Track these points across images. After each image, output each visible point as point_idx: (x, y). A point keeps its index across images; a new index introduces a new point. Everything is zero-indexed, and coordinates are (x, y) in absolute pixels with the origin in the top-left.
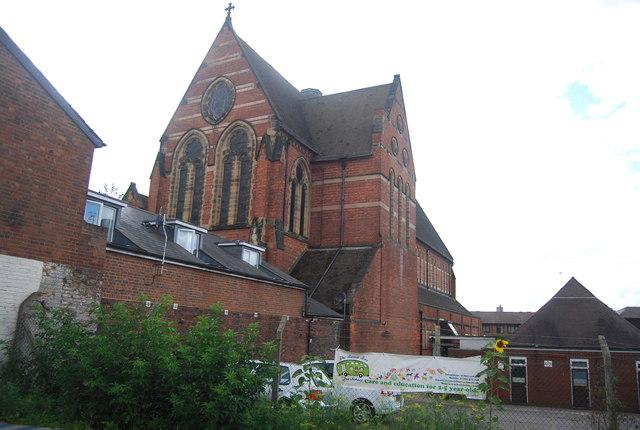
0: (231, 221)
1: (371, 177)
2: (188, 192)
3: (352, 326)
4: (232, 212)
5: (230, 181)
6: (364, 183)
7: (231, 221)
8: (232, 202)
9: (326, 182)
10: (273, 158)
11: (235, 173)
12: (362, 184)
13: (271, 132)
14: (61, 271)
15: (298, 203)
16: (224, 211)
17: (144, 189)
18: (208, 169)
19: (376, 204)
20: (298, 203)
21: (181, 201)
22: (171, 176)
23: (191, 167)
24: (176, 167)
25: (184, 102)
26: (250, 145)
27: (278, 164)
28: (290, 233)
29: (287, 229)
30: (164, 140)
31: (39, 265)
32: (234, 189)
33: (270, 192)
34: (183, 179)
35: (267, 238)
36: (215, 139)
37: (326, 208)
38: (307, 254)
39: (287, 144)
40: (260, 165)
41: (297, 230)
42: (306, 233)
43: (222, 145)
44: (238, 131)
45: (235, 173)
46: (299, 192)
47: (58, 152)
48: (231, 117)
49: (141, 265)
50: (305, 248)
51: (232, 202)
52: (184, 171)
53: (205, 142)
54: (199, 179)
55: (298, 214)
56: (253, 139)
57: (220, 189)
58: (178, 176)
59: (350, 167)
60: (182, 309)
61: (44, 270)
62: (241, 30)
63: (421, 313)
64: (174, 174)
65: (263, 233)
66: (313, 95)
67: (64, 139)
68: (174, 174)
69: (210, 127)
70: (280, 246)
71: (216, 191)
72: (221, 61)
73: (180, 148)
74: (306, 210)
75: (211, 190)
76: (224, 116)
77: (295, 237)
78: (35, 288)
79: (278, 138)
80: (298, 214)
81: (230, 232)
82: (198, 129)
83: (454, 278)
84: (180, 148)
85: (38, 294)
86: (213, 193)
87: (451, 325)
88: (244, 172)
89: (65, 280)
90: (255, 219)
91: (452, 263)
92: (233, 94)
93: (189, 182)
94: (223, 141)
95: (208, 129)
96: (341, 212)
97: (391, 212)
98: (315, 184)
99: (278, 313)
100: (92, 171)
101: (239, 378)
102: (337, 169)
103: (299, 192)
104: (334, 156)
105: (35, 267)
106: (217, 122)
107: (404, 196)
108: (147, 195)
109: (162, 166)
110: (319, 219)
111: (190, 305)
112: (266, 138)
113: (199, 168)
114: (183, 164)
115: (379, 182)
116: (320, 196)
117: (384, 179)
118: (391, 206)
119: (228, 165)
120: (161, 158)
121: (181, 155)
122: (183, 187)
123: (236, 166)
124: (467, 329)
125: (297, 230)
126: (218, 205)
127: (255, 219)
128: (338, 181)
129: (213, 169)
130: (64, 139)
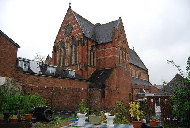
0: (73, 63)
1: (112, 48)
2: (62, 56)
3: (106, 91)
4: (73, 61)
5: (72, 52)
6: (110, 49)
7: (73, 63)
8: (73, 58)
9: (100, 50)
10: (83, 45)
11: (74, 50)
12: (110, 50)
13: (82, 37)
14: (10, 79)
15: (92, 57)
16: (71, 61)
17: (51, 56)
18: (67, 49)
19: (114, 55)
20: (92, 57)
21: (60, 59)
22: (57, 52)
23: (62, 49)
24: (58, 49)
25: (60, 31)
26: (77, 42)
27: (84, 47)
28: (93, 67)
29: (89, 64)
30: (55, 42)
31: (168, 83)
32: (73, 54)
33: (82, 54)
34: (61, 52)
35: (82, 67)
36: (68, 41)
37: (100, 58)
38: (95, 72)
39: (88, 40)
40: (79, 47)
41: (92, 64)
42: (95, 65)
43: (70, 42)
44: (74, 38)
45: (74, 50)
46: (92, 53)
47: (8, 50)
48: (72, 34)
49: (34, 76)
50: (95, 70)
51: (73, 58)
52: (61, 50)
53: (65, 42)
54: (64, 52)
55: (92, 60)
56: (77, 40)
57: (70, 55)
58: (59, 52)
59: (106, 45)
60: (48, 88)
61: (6, 79)
62: (73, 9)
63: (132, 86)
64: (58, 51)
65: (81, 66)
66: (98, 25)
67: (9, 47)
68: (58, 51)
69: (67, 38)
70: (86, 69)
71: (69, 55)
72: (68, 19)
73: (59, 44)
74: (95, 59)
75: (67, 55)
76: (70, 34)
77: (91, 67)
78: (4, 83)
79: (84, 39)
80: (92, 60)
81: (73, 66)
82: (63, 38)
83: (148, 76)
84: (59, 44)
85: (4, 85)
86: (68, 56)
87: (144, 90)
88: (76, 49)
89: (11, 81)
90: (79, 62)
91: (148, 71)
92: (72, 28)
93: (62, 53)
94: (70, 41)
95: (66, 38)
96: (105, 59)
97: (120, 58)
98: (97, 51)
99: (53, 86)
100: (17, 54)
101: (180, 114)
102: (103, 46)
103: (92, 53)
104: (101, 42)
105: (3, 78)
106: (68, 36)
107: (124, 52)
108: (52, 57)
109: (55, 50)
110: (98, 61)
111: (50, 86)
112: (81, 39)
113: (64, 49)
114: (60, 49)
115: (115, 49)
116: (99, 54)
117: (116, 48)
118: (119, 56)
119: (71, 47)
120: (55, 47)
121: (60, 46)
122: (60, 54)
123: (73, 48)
124: (151, 90)
125: (92, 64)
126: (70, 59)
127: (79, 62)
128: (104, 49)
129: (68, 49)
130: (9, 47)
